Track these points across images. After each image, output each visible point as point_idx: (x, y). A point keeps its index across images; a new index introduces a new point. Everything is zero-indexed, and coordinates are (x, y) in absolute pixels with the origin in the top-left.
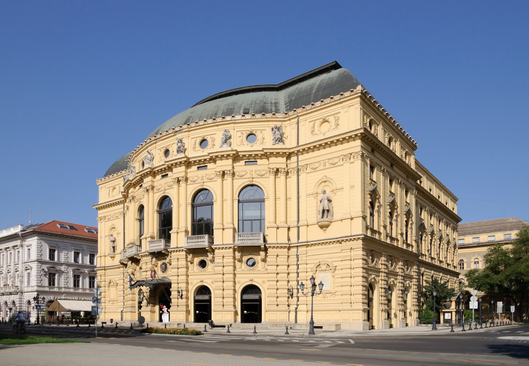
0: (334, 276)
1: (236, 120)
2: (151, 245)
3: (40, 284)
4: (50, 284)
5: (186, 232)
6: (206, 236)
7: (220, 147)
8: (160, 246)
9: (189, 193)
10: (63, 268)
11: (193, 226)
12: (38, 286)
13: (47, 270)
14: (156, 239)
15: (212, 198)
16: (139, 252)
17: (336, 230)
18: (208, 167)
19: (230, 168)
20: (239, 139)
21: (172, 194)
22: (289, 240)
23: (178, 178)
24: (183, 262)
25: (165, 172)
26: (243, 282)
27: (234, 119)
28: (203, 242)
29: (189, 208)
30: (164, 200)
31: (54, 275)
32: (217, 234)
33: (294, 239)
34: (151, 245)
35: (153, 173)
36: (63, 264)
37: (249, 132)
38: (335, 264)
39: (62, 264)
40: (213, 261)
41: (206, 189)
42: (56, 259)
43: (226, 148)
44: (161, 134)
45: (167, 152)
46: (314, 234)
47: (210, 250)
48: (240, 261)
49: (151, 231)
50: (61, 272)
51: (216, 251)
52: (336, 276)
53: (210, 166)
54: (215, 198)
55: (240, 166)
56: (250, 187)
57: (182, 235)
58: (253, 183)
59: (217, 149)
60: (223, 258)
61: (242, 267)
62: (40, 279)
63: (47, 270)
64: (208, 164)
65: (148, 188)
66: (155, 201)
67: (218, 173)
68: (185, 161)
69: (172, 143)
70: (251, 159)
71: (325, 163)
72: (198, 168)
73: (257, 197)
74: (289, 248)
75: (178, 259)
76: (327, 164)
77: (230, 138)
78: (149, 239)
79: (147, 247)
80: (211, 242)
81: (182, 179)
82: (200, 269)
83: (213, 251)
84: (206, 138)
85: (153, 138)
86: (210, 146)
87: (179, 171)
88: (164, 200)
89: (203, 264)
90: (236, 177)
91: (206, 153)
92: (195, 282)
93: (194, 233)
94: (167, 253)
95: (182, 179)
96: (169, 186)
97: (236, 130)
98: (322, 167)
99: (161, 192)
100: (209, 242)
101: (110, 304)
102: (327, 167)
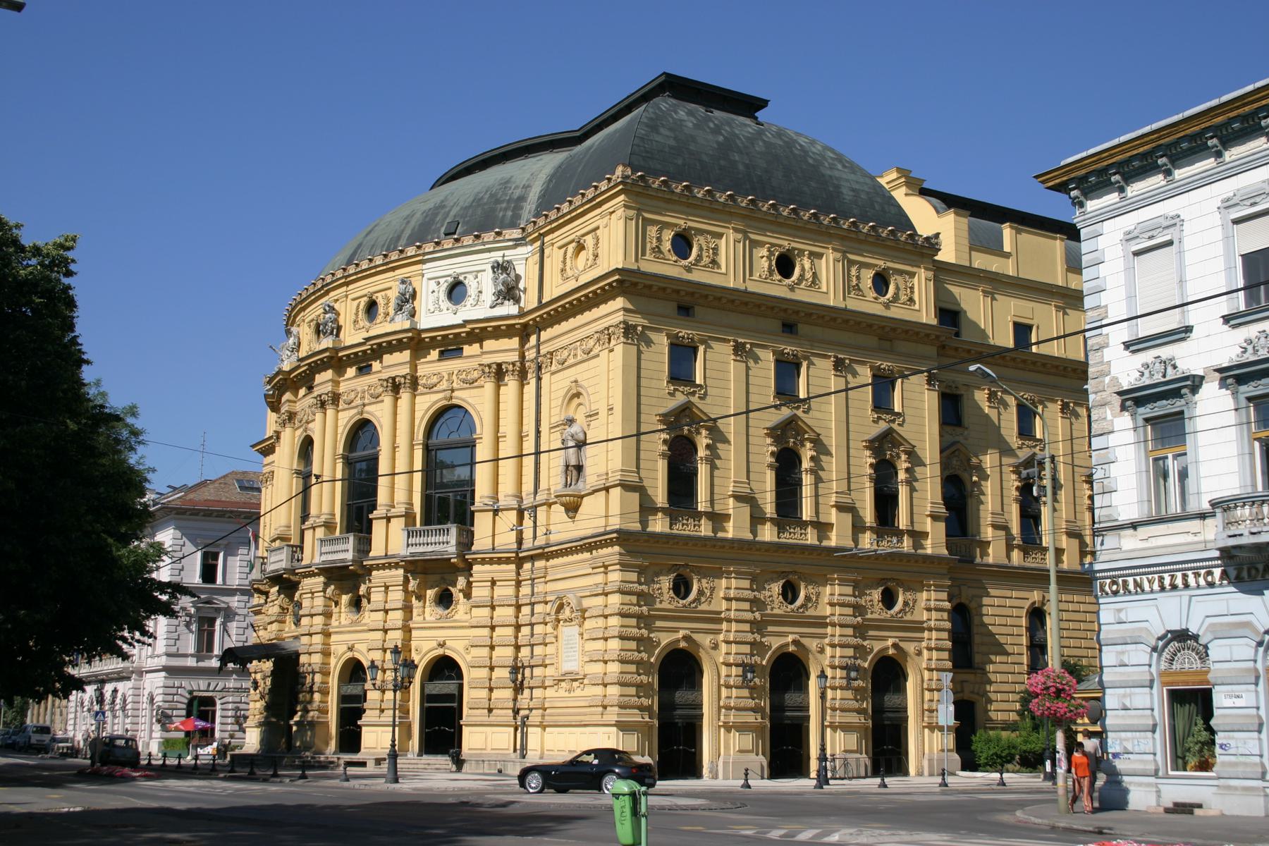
1: (424, 254)
2: (325, 549)
3: (173, 650)
4: (199, 648)
5: (409, 516)
6: (454, 530)
7: (492, 307)
8: (346, 552)
9: (418, 415)
10: (235, 602)
11: (427, 500)
12: (168, 655)
13: (193, 610)
14: (338, 533)
15: (472, 429)
16: (296, 564)
18: (465, 353)
19: (514, 357)
20: (432, 298)
21: (380, 413)
22: (520, 541)
23: (394, 379)
24: (397, 596)
25: (362, 361)
26: (424, 650)
27: (421, 252)
28: (445, 543)
30: (362, 431)
31: (212, 621)
32: (482, 524)
34: (325, 549)
35: (336, 361)
36: (236, 590)
39: (231, 592)
40: (468, 595)
41: (460, 407)
42: (219, 580)
43: (509, 309)
44: (357, 265)
45: (371, 307)
47: (461, 565)
48: (421, 597)
49: (325, 509)
50: (229, 614)
51: (476, 568)
52: (586, 636)
54: (478, 431)
55: (431, 366)
57: (398, 525)
58: (455, 401)
61: (426, 612)
62: (175, 635)
63: (193, 610)
65: (324, 397)
66: (340, 430)
67: (487, 370)
68: (411, 339)
69: (387, 286)
72: (441, 353)
73: (464, 436)
75: (387, 587)
77: (414, 295)
78: (320, 533)
79: (314, 554)
80: (466, 541)
81: (402, 380)
82: (440, 611)
83: (467, 568)
84: (461, 278)
85: (339, 274)
86: (470, 301)
87: (396, 364)
88: (362, 431)
89: (445, 600)
90: (420, 389)
91: (458, 320)
92: (426, 646)
93: (427, 520)
94: (360, 572)
95: (402, 380)
96: (371, 396)
97: (426, 276)
98: (571, 361)
99: (355, 411)
100: (459, 544)
101: (562, 693)
102: (579, 358)
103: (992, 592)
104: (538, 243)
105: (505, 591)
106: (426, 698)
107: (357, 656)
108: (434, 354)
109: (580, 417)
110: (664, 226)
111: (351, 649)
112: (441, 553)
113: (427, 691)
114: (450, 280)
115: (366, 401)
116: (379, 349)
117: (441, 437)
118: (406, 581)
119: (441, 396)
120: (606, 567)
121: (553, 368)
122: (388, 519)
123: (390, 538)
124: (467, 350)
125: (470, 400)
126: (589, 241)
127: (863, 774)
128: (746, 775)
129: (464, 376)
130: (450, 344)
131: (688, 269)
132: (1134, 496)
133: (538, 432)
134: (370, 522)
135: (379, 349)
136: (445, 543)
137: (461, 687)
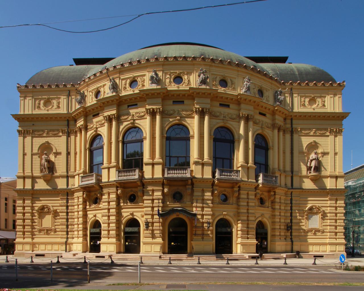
6: (137, 171)
24: (113, 196)
34: (84, 180)
38: (55, 208)
54: (144, 135)
56: (133, 129)
57: (113, 171)
60: (110, 196)
73: (138, 137)
103: (37, 202)
106: (91, 234)
107: (97, 218)
110: (41, 99)
111: (95, 216)
113: (91, 232)
117: (129, 138)
118: (84, 194)
119: (93, 131)
120: (78, 197)
122: (109, 168)
125: (101, 131)
127: (122, 250)
129: (100, 123)
131: (48, 110)
137: (100, 230)
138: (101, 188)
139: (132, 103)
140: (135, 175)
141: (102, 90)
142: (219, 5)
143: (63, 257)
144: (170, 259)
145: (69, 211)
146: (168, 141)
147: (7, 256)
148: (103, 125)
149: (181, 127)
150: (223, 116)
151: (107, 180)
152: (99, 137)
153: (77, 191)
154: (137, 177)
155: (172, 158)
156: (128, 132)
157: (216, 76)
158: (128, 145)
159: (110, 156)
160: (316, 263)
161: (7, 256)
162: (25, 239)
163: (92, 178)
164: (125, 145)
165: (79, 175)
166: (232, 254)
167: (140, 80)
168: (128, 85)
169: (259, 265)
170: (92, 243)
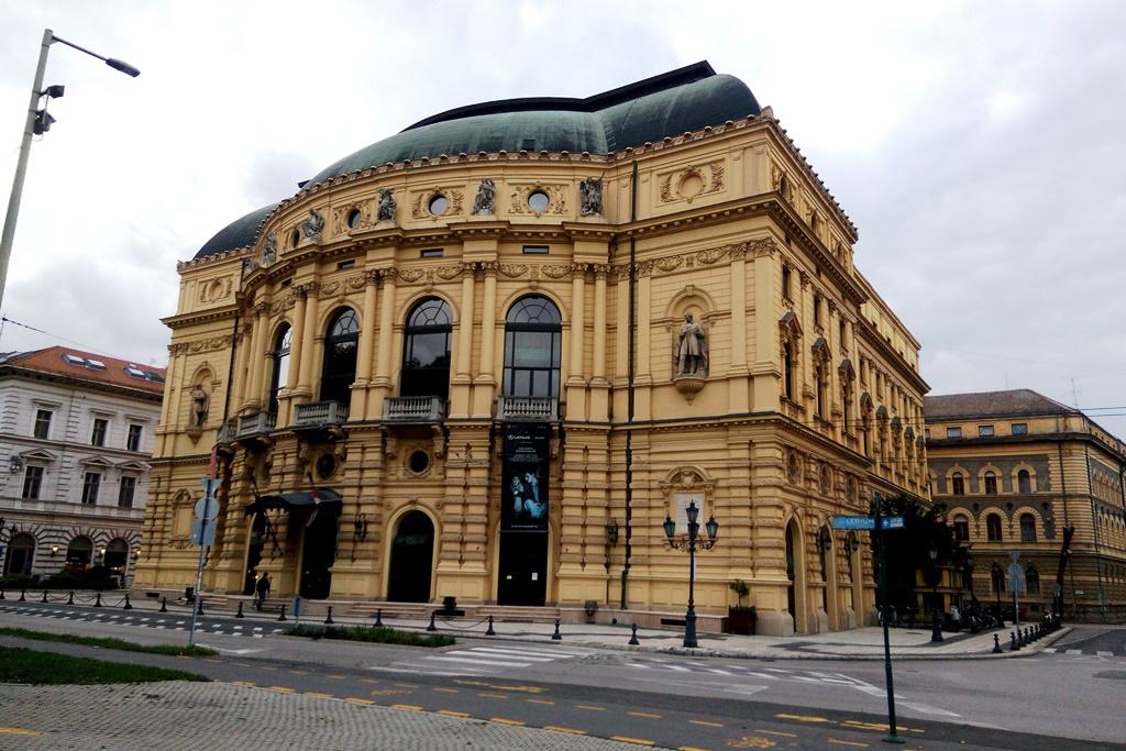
0: (710, 503)
17: (717, 402)
18: (445, 253)
23: (377, 271)
25: (345, 256)
29: (399, 337)
33: (621, 415)
37: (532, 188)
40: (443, 456)
46: (669, 406)
53: (448, 251)
55: (413, 263)
56: (530, 301)
58: (346, 304)
59: (466, 216)
64: (551, 246)
70: (430, 244)
71: (692, 259)
72: (423, 252)
73: (441, 320)
74: (611, 434)
76: (695, 262)
84: (357, 207)
87: (381, 259)
89: (419, 463)
98: (685, 269)
101: (173, 549)
102: (696, 267)
104: (631, 169)
105: (598, 458)
108: (334, 267)
109: (696, 314)
112: (426, 420)
114: (431, 193)
115: (348, 291)
116: (359, 248)
117: (420, 320)
118: (299, 449)
120: (285, 454)
121: (654, 273)
122: (368, 390)
123: (369, 405)
124: (553, 249)
125: (557, 292)
126: (707, 172)
128: (330, 612)
129: (443, 273)
130: (535, 240)
132: (554, 445)
133: (632, 327)
134: (349, 392)
135: (359, 248)
136: (330, 415)
138: (346, 433)
139: (430, 245)
140: (433, 411)
141: (364, 210)
142: (82, 47)
143: (619, 621)
144: (283, 609)
145: (631, 504)
146: (510, 334)
147: (996, 636)
148: (363, 289)
149: (542, 302)
150: (426, 276)
151: (360, 418)
152: (350, 313)
153: (283, 438)
154: (434, 416)
155: (518, 373)
156: (419, 310)
157: (419, 194)
158: (416, 337)
159: (380, 359)
160: (495, 630)
161: (996, 636)
162: (466, 564)
163: (325, 412)
164: (410, 337)
165: (290, 399)
166: (427, 602)
167: (451, 197)
168: (423, 206)
169: (334, 625)
170: (535, 577)
